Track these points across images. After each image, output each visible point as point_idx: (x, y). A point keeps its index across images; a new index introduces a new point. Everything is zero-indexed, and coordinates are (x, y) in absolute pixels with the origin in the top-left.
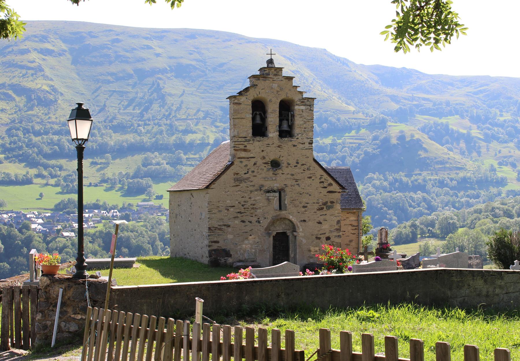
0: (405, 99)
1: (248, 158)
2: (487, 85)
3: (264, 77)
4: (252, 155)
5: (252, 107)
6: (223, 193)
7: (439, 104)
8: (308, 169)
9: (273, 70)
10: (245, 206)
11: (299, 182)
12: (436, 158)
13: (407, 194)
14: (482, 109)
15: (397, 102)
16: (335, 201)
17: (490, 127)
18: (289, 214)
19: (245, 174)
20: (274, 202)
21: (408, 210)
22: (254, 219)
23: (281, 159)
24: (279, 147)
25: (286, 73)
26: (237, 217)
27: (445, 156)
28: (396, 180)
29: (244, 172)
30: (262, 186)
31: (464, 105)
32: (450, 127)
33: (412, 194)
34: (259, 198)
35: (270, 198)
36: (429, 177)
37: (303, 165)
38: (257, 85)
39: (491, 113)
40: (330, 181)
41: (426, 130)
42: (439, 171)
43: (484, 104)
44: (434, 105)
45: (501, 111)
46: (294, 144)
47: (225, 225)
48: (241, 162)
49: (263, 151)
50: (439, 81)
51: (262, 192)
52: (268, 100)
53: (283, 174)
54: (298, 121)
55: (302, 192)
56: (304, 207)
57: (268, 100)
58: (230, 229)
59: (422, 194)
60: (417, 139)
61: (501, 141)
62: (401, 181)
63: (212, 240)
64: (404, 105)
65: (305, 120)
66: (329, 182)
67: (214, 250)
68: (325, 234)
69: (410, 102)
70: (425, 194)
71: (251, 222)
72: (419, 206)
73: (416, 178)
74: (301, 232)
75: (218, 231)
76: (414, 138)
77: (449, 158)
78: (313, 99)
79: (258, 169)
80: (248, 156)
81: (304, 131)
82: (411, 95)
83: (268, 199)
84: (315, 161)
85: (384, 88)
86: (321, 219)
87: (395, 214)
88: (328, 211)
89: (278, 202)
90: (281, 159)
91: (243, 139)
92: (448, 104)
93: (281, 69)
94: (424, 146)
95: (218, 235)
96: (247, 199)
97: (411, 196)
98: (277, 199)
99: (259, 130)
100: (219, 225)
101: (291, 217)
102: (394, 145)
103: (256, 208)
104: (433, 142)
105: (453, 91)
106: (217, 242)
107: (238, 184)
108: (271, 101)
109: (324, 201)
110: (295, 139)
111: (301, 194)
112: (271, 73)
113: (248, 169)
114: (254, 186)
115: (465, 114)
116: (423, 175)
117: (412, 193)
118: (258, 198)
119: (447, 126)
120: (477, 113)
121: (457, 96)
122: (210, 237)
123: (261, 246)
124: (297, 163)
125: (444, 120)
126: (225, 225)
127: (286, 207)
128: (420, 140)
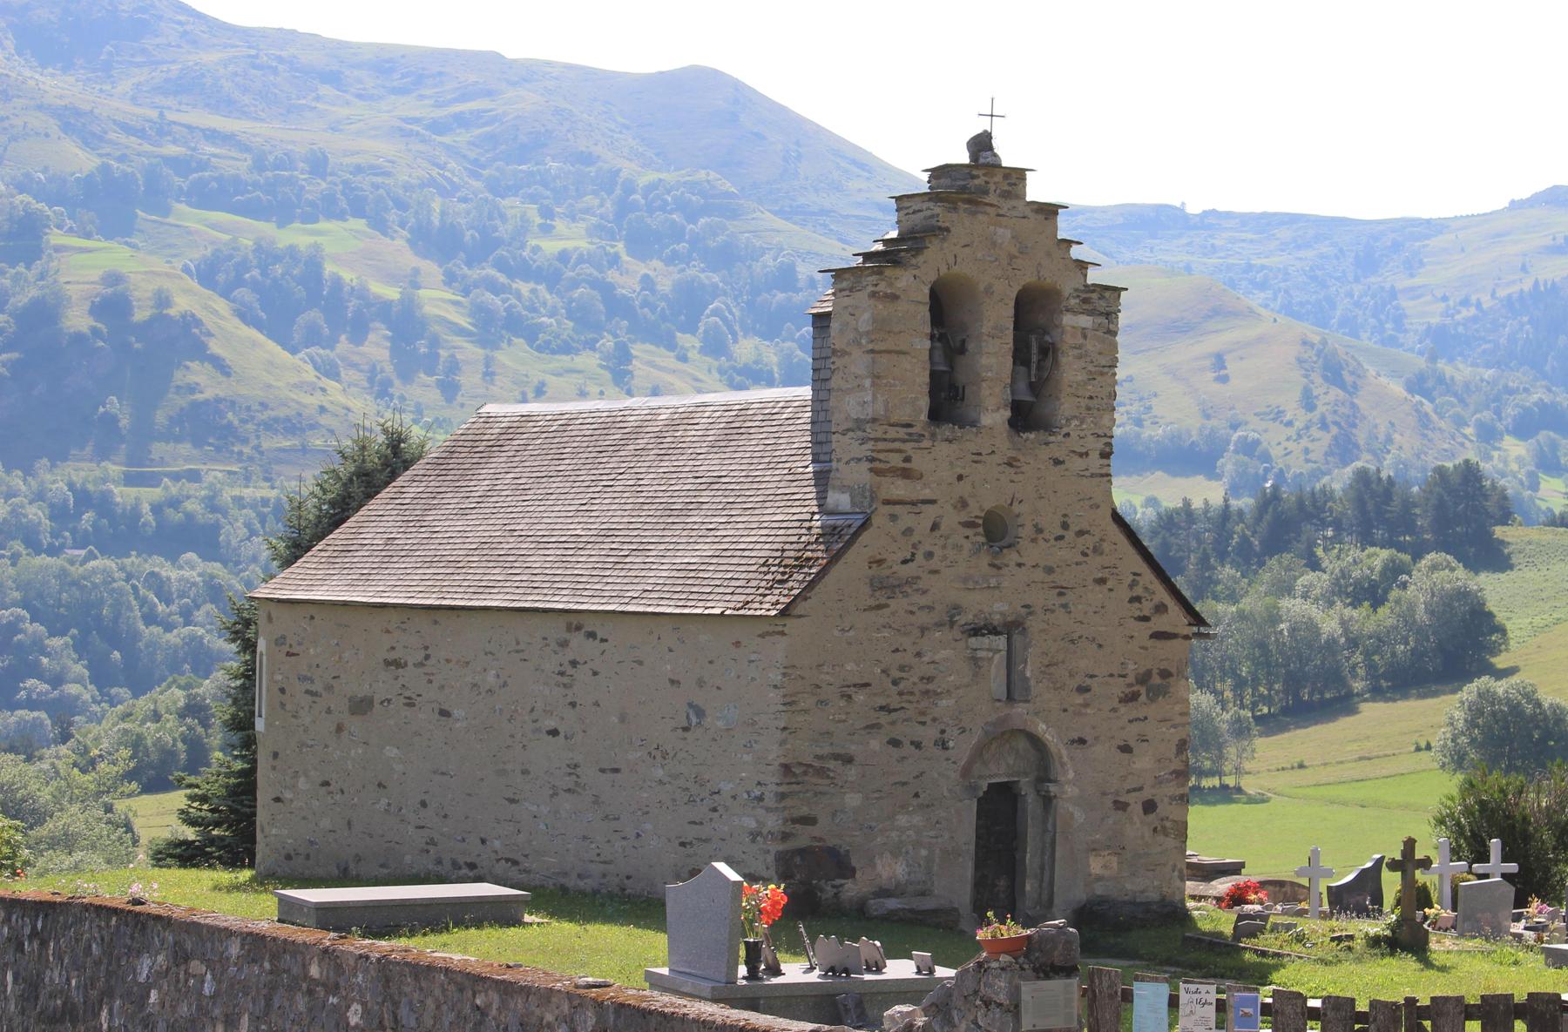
0: (127, 129)
1: (913, 504)
2: (490, 94)
3: (969, 201)
4: (926, 493)
5: (931, 310)
6: (836, 633)
7: (279, 165)
8: (1095, 550)
9: (998, 178)
10: (902, 686)
11: (1070, 597)
12: (264, 406)
13: (132, 560)
14: (464, 200)
15: (90, 140)
16: (1174, 670)
17: (502, 278)
18: (1036, 714)
19: (905, 562)
20: (993, 670)
21: (136, 636)
22: (929, 734)
23: (1016, 508)
24: (1010, 465)
25: (1036, 191)
26: (877, 726)
27: (308, 400)
28: (84, 499)
29: (901, 556)
30: (957, 609)
31: (387, 174)
32: (329, 268)
33: (159, 565)
34: (945, 651)
35: (980, 654)
36: (236, 492)
37: (1081, 533)
38: (948, 230)
39: (503, 217)
40: (1162, 595)
41: (221, 277)
42: (279, 461)
43: (477, 176)
44: (259, 165)
45: (547, 213)
46: (1057, 455)
47: (836, 757)
48: (893, 518)
49: (960, 478)
50: (280, 59)
51: (956, 633)
52: (981, 287)
53: (1020, 565)
54: (1071, 371)
55: (1075, 636)
56: (1083, 690)
57: (981, 287)
58: (852, 773)
59: (202, 566)
60: (184, 316)
61: (548, 343)
62: (104, 504)
63: (796, 814)
64: (121, 159)
65: (1091, 368)
66: (1156, 600)
67: (802, 852)
68: (1141, 789)
69: (147, 147)
70: (215, 568)
71: (917, 745)
72: (187, 623)
73: (174, 490)
74: (1069, 788)
75: (814, 780)
76: (172, 312)
77: (322, 409)
78: (1117, 291)
79: (944, 547)
80: (914, 497)
81: (1089, 409)
82: (154, 114)
83: (975, 660)
84: (1117, 518)
85: (28, 73)
86: (1131, 733)
87: (81, 647)
88: (1153, 706)
89: (1004, 672)
90: (1016, 508)
91: (902, 432)
92: (318, 165)
93: (1018, 175)
94: (215, 347)
95: (816, 794)
96: (908, 658)
97: (152, 574)
98: (999, 659)
99: (947, 402)
100: (818, 757)
101: (1041, 728)
102: (79, 338)
103: (936, 694)
104: (253, 333)
105: (344, 112)
106: (809, 821)
107: (883, 601)
108: (989, 291)
109: (1142, 670)
110: (1060, 438)
111: (1072, 641)
112: (992, 187)
113: (914, 546)
114: (931, 608)
115: (393, 216)
116: (209, 478)
117: (158, 559)
118: (944, 654)
119: (313, 263)
120: (443, 213)
121: (360, 136)
122: (788, 802)
123: (947, 836)
124: (1065, 526)
125: (295, 237)
126: (836, 757)
127: (1028, 689)
128: (198, 323)
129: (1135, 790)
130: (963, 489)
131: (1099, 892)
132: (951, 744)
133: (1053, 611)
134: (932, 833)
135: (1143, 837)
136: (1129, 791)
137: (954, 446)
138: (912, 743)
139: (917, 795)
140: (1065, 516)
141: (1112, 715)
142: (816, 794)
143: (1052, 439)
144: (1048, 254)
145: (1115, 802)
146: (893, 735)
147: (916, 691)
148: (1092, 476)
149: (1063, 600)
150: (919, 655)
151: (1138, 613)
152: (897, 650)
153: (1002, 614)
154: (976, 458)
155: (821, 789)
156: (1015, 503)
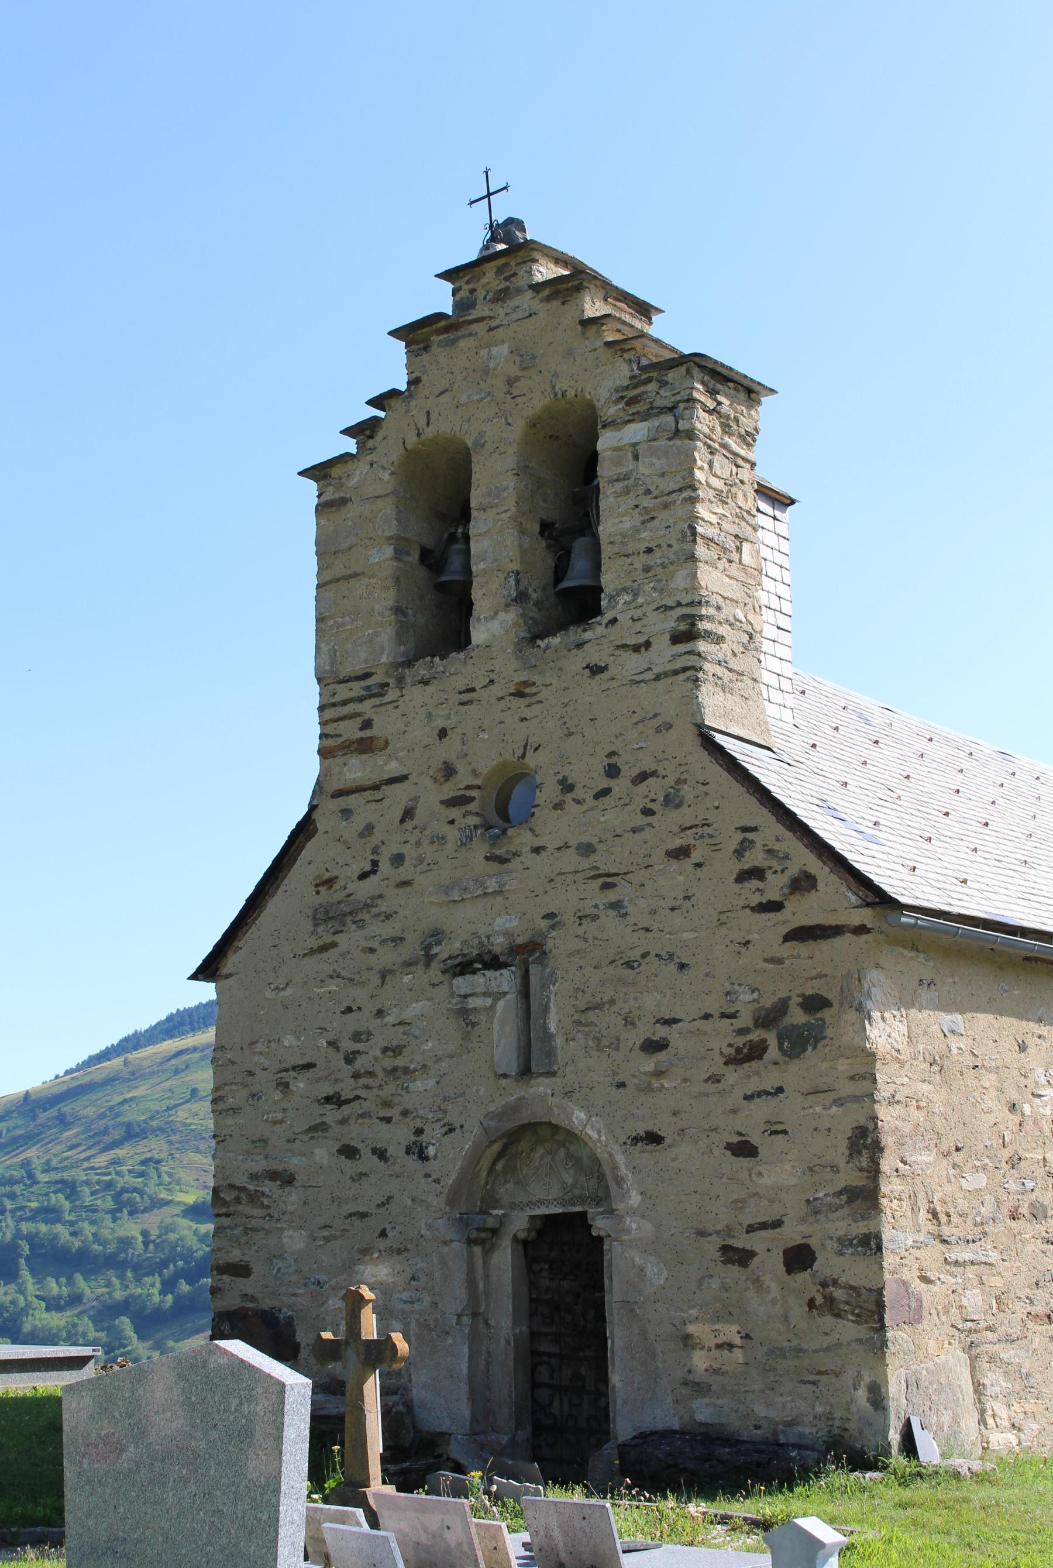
1: (376, 787)
4: (393, 768)
6: (269, 994)
8: (667, 801)
10: (360, 1063)
11: (622, 891)
16: (832, 996)
18: (568, 1094)
19: (363, 876)
24: (519, 694)
25: (392, 369)
29: (356, 868)
34: (420, 1004)
37: (642, 777)
47: (273, 1175)
48: (346, 813)
49: (443, 733)
51: (435, 973)
53: (537, 850)
56: (653, 1046)
58: (293, 1198)
65: (647, 502)
66: (793, 870)
68: (777, 1224)
79: (418, 843)
80: (376, 777)
81: (647, 569)
83: (464, 1014)
86: (750, 1123)
88: (794, 1066)
90: (531, 760)
91: (357, 688)
96: (364, 1020)
98: (506, 1009)
99: (441, 616)
100: (254, 1177)
103: (406, 1071)
107: (328, 939)
109: (768, 1002)
111: (629, 965)
114: (398, 940)
118: (415, 1009)
123: (427, 1299)
124: (612, 771)
126: (273, 1175)
127: (550, 1054)
129: (763, 1226)
130: (448, 751)
131: (700, 1417)
132: (431, 1151)
133: (595, 918)
134: (405, 1296)
135: (785, 1318)
136: (751, 1229)
137: (430, 689)
138: (374, 1151)
139: (383, 1234)
140: (612, 754)
141: (711, 1088)
142: (246, 1231)
143: (588, 635)
144: (569, 353)
145: (725, 1249)
146: (345, 1141)
147: (378, 1070)
148: (658, 678)
149: (612, 896)
150: (380, 1013)
151: (756, 899)
152: (349, 1010)
153: (506, 933)
154: (466, 697)
155: (254, 1223)
156: (529, 753)
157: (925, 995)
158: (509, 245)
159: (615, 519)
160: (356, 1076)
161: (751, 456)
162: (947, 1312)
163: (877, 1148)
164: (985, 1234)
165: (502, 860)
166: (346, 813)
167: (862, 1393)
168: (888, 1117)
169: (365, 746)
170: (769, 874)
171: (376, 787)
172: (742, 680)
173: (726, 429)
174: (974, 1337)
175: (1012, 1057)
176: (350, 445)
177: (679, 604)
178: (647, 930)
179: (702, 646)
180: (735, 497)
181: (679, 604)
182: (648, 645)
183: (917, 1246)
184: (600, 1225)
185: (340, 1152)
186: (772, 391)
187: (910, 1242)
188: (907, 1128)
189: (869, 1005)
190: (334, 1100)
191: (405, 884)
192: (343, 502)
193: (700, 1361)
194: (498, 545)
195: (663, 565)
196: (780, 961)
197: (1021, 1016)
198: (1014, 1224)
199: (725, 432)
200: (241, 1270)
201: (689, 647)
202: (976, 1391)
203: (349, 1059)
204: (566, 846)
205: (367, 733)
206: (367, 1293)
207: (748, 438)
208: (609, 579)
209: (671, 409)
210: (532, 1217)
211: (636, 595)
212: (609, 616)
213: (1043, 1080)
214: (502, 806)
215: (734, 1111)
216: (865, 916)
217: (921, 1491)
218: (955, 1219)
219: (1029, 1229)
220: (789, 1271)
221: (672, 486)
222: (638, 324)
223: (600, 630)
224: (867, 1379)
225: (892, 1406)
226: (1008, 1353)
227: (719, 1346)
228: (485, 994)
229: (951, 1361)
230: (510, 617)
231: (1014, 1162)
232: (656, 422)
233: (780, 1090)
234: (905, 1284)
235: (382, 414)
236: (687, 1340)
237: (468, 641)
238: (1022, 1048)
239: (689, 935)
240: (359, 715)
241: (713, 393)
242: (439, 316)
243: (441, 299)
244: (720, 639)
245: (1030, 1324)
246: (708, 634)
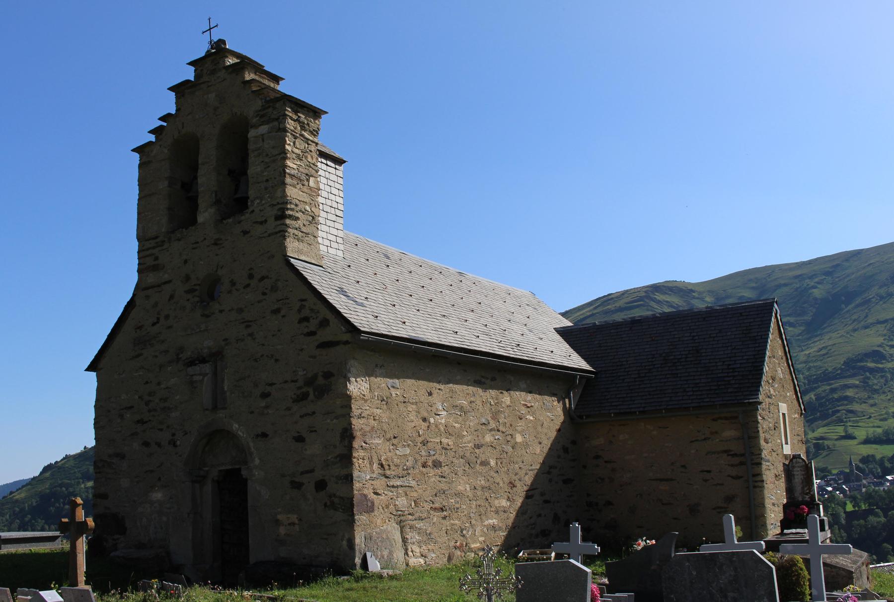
1: (159, 286)
19: (154, 324)
24: (216, 244)
37: (263, 278)
49: (186, 262)
53: (221, 311)
56: (265, 395)
65: (267, 160)
68: (312, 471)
111: (256, 360)
114: (166, 352)
124: (251, 276)
132: (178, 443)
133: (243, 340)
136: (302, 473)
138: (156, 443)
140: (251, 269)
143: (243, 218)
145: (292, 482)
150: (159, 384)
151: (306, 330)
152: (147, 383)
154: (195, 246)
157: (378, 371)
158: (219, 49)
159: (254, 168)
160: (149, 411)
161: (316, 140)
162: (387, 507)
163: (352, 437)
164: (409, 474)
165: (208, 316)
166: (147, 297)
167: (345, 543)
168: (356, 423)
169: (155, 268)
170: (311, 320)
171: (159, 286)
172: (309, 236)
173: (303, 128)
174: (402, 518)
175: (424, 398)
176: (152, 138)
177: (278, 203)
178: (263, 345)
179: (288, 221)
180: (306, 157)
181: (278, 203)
182: (266, 221)
183: (372, 479)
184: (244, 473)
185: (143, 444)
186: (326, 113)
187: (368, 477)
188: (368, 429)
189: (349, 375)
190: (141, 422)
191: (170, 327)
192: (149, 162)
193: (282, 531)
194: (208, 180)
195: (272, 187)
196: (314, 357)
197: (429, 381)
198: (424, 470)
199: (302, 129)
200: (104, 496)
201: (282, 222)
202: (403, 541)
203: (147, 404)
204: (232, 309)
205: (156, 262)
206: (79, 501)
207: (315, 133)
208: (252, 193)
209: (277, 119)
210: (220, 471)
211: (261, 200)
212: (251, 209)
213: (440, 408)
214: (208, 292)
215: (296, 423)
216: (347, 337)
217: (366, 583)
218: (393, 467)
219: (432, 472)
220: (317, 491)
221: (277, 152)
222: (272, 85)
223: (247, 215)
224: (347, 537)
225: (357, 548)
226: (420, 525)
227: (289, 524)
228: (200, 374)
229: (390, 528)
230: (212, 210)
231: (424, 443)
232: (271, 125)
233: (314, 413)
234: (365, 496)
235: (165, 124)
236: (277, 522)
237: (196, 221)
238: (430, 394)
239: (279, 347)
240: (153, 254)
241: (296, 112)
242: (188, 81)
243: (189, 74)
244: (297, 219)
245: (432, 512)
246: (290, 217)
